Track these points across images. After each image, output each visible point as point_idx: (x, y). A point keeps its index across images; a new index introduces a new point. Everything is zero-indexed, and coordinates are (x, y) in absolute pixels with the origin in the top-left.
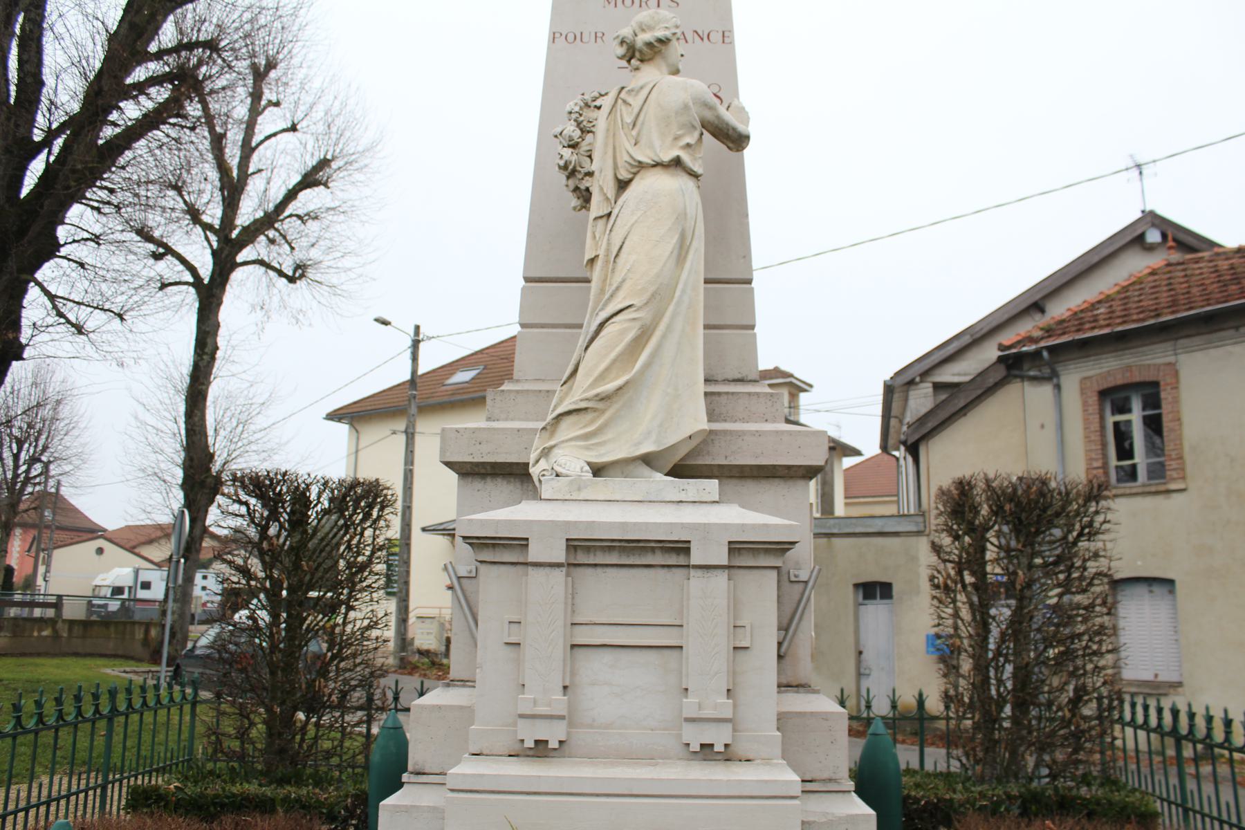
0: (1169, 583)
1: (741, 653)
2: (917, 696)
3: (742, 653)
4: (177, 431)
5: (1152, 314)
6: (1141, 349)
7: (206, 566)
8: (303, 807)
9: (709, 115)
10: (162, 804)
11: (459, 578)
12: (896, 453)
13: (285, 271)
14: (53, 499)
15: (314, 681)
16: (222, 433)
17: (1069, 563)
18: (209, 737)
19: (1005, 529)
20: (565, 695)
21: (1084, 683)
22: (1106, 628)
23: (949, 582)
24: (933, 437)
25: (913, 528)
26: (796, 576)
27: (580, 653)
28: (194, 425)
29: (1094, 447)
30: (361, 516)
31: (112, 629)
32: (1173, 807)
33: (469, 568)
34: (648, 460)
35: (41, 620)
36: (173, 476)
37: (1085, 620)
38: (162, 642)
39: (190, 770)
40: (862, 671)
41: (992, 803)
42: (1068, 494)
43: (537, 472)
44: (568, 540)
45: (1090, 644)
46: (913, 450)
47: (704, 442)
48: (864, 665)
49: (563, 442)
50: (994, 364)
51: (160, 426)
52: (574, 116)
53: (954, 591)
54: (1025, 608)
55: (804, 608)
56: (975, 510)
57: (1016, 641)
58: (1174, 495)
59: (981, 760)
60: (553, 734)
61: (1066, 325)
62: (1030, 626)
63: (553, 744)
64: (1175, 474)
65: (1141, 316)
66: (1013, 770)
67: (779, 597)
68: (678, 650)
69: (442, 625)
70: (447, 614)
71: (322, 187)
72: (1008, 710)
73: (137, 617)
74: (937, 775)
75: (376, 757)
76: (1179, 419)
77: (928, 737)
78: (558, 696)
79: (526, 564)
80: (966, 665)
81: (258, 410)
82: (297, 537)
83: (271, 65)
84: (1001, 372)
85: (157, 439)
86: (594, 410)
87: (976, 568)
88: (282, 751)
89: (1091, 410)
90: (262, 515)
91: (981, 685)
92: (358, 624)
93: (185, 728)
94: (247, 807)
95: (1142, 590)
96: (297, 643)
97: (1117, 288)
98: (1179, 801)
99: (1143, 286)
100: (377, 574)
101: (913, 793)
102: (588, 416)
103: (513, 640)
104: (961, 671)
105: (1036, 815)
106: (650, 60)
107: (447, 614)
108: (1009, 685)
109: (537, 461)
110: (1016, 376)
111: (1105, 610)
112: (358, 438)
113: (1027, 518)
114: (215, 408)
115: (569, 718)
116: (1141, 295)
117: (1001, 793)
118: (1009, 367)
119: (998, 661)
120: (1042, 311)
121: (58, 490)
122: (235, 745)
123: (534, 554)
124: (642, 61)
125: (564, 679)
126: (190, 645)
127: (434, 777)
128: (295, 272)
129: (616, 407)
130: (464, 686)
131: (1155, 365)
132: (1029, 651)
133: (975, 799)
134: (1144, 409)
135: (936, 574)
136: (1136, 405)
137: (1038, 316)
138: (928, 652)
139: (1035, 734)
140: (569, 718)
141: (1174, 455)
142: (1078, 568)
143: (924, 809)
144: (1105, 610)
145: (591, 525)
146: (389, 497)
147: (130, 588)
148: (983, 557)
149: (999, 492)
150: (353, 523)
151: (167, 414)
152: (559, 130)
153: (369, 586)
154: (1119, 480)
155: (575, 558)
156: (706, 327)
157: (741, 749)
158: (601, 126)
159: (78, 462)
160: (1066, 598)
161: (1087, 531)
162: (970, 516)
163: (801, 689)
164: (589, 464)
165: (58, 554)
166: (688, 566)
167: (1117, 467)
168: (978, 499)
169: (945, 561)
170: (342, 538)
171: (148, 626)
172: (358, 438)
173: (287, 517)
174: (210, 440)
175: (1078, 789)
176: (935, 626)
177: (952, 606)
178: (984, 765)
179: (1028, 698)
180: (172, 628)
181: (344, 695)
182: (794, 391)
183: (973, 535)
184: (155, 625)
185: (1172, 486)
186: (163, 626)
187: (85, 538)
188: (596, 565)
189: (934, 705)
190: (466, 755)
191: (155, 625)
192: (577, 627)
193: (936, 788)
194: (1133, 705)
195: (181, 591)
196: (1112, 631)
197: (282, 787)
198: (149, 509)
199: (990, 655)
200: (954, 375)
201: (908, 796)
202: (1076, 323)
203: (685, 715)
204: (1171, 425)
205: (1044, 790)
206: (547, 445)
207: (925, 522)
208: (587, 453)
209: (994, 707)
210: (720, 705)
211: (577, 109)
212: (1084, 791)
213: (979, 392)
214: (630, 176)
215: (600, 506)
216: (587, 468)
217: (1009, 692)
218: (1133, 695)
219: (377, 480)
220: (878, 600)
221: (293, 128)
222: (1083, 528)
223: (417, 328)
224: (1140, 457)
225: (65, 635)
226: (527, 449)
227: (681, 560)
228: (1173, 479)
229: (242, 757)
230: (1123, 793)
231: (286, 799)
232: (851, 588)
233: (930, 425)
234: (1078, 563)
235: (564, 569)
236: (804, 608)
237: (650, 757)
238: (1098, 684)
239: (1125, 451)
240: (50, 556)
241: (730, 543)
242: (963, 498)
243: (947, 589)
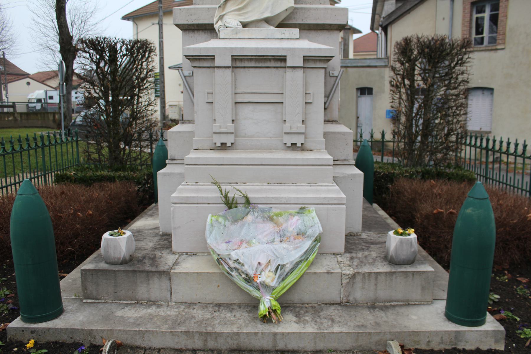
0: (491, 90)
1: (308, 106)
2: (382, 132)
3: (309, 105)
4: (54, 26)
7: (76, 88)
8: (127, 179)
10: (69, 180)
11: (185, 77)
12: (377, 32)
14: (3, 60)
15: (127, 128)
16: (75, 26)
17: (451, 76)
18: (85, 153)
19: (424, 60)
20: (233, 124)
21: (452, 127)
22: (464, 104)
23: (398, 84)
25: (383, 64)
26: (332, 74)
27: (239, 105)
28: (61, 23)
29: (466, 29)
30: (141, 56)
31: (39, 116)
32: (482, 177)
33: (189, 72)
34: (267, 21)
35: (8, 113)
36: (56, 47)
37: (455, 101)
38: (61, 121)
39: (80, 167)
40: (359, 125)
41: (410, 174)
42: (453, 45)
43: (218, 26)
44: (232, 56)
45: (456, 111)
46: (385, 29)
48: (359, 122)
49: (229, 12)
51: (46, 24)
53: (400, 88)
54: (430, 95)
55: (336, 88)
56: (411, 51)
57: (425, 109)
58: (499, 51)
59: (407, 158)
60: (228, 140)
62: (431, 103)
63: (229, 144)
64: (500, 42)
66: (419, 161)
67: (325, 83)
68: (282, 104)
69: (180, 109)
70: (182, 103)
72: (419, 138)
73: (49, 111)
74: (388, 164)
75: (155, 158)
76: (506, 16)
77: (385, 153)
78: (230, 124)
79: (214, 67)
80: (403, 119)
81: (90, 15)
82: (113, 67)
85: (45, 30)
87: (410, 77)
88: (116, 158)
89: (466, 11)
90: (96, 57)
91: (409, 127)
92: (143, 104)
93: (75, 153)
94: (104, 180)
95: (479, 93)
96: (117, 113)
98: (484, 175)
100: (150, 82)
101: (378, 170)
103: (210, 101)
104: (401, 121)
105: (428, 178)
107: (182, 103)
108: (421, 128)
109: (217, 22)
111: (464, 97)
112: (137, 28)
113: (434, 56)
114: (70, 15)
115: (235, 133)
117: (414, 170)
119: (417, 117)
121: (4, 56)
122: (96, 156)
125: (232, 117)
126: (73, 121)
127: (179, 161)
132: (430, 114)
133: (404, 173)
134: (491, 11)
135: (392, 80)
138: (386, 117)
139: (430, 147)
140: (235, 133)
141: (501, 32)
142: (454, 78)
143: (382, 177)
144: (464, 97)
145: (242, 49)
146: (152, 48)
147: (44, 99)
148: (414, 78)
149: (423, 44)
150: (137, 60)
151: (48, 18)
153: (147, 87)
154: (475, 44)
155: (236, 64)
157: (308, 145)
159: (11, 43)
160: (448, 92)
161: (460, 62)
162: (409, 54)
163: (334, 123)
164: (241, 22)
165: (10, 85)
166: (285, 67)
167: (475, 39)
168: (413, 47)
169: (397, 74)
170: (133, 66)
171: (54, 114)
172: (137, 28)
173: (108, 58)
174: (70, 30)
175: (445, 170)
176: (391, 102)
177: (398, 94)
178: (408, 160)
179: (428, 133)
180: (64, 114)
181: (140, 134)
183: (410, 63)
184: (57, 113)
185: (499, 47)
186: (61, 114)
187: (20, 78)
188: (245, 67)
189: (389, 137)
190: (192, 150)
191: (57, 113)
192: (237, 94)
193: (388, 168)
194: (482, 140)
195: (66, 98)
196: (466, 106)
197: (117, 172)
198: (47, 63)
199: (414, 115)
201: (376, 171)
203: (284, 131)
204: (502, 18)
205: (431, 170)
206: (222, 14)
207: (388, 61)
208: (240, 17)
209: (414, 136)
210: (299, 127)
212: (447, 171)
213: (416, 2)
215: (245, 41)
216: (240, 24)
217: (420, 130)
219: (146, 40)
220: (367, 95)
222: (458, 61)
224: (486, 34)
225: (19, 119)
226: (213, 17)
227: (282, 65)
228: (500, 44)
229: (100, 161)
230: (463, 171)
231: (119, 177)
232: (355, 90)
233: (393, 18)
234: (454, 76)
235: (231, 69)
236: (336, 88)
237: (269, 149)
238: (458, 128)
239: (479, 30)
240: (6, 87)
241: (304, 56)
242: (407, 46)
243: (397, 87)
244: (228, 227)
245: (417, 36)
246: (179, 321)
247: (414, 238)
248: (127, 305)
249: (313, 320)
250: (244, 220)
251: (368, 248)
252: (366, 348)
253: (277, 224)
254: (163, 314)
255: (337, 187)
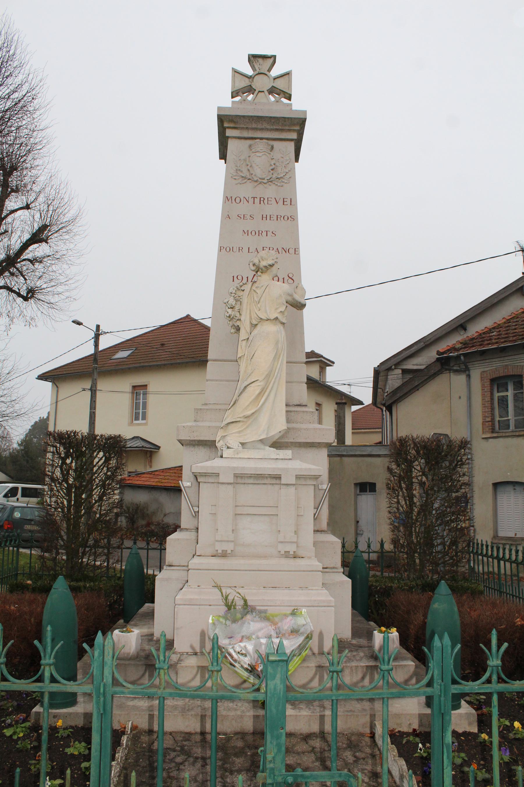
5: (520, 337)
6: (516, 357)
9: (289, 299)
13: (22, 293)
24: (402, 403)
46: (389, 409)
47: (286, 433)
50: (435, 361)
52: (233, 295)
60: (229, 547)
61: (475, 341)
65: (514, 338)
71: (44, 244)
79: (219, 483)
83: (14, 168)
84: (438, 366)
86: (243, 421)
95: (510, 488)
97: (504, 320)
99: (518, 319)
102: (241, 424)
106: (266, 272)
109: (219, 441)
110: (446, 370)
112: (58, 391)
116: (516, 325)
118: (442, 364)
120: (465, 329)
123: (222, 479)
124: (262, 273)
128: (28, 294)
129: (251, 420)
130: (187, 531)
131: (520, 366)
134: (514, 390)
135: (389, 482)
136: (510, 387)
137: (462, 332)
152: (226, 301)
156: (287, 382)
158: (245, 300)
164: (240, 443)
166: (280, 484)
167: (499, 421)
172: (58, 391)
182: (322, 365)
200: (413, 365)
201: (372, 585)
202: (480, 340)
211: (234, 292)
213: (426, 377)
214: (257, 323)
216: (240, 445)
218: (504, 545)
221: (27, 207)
223: (98, 327)
227: (278, 481)
232: (353, 485)
233: (399, 395)
244: (229, 626)
245: (412, 436)
246: (187, 708)
247: (396, 635)
248: (135, 698)
249: (307, 707)
250: (243, 619)
251: (357, 650)
252: (354, 730)
253: (274, 623)
254: (171, 704)
255: (326, 591)
